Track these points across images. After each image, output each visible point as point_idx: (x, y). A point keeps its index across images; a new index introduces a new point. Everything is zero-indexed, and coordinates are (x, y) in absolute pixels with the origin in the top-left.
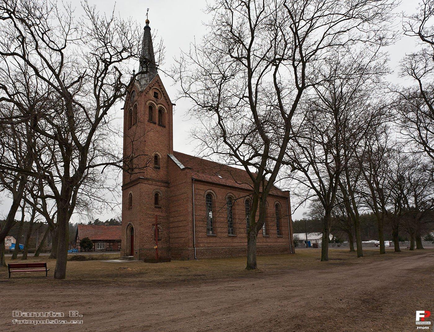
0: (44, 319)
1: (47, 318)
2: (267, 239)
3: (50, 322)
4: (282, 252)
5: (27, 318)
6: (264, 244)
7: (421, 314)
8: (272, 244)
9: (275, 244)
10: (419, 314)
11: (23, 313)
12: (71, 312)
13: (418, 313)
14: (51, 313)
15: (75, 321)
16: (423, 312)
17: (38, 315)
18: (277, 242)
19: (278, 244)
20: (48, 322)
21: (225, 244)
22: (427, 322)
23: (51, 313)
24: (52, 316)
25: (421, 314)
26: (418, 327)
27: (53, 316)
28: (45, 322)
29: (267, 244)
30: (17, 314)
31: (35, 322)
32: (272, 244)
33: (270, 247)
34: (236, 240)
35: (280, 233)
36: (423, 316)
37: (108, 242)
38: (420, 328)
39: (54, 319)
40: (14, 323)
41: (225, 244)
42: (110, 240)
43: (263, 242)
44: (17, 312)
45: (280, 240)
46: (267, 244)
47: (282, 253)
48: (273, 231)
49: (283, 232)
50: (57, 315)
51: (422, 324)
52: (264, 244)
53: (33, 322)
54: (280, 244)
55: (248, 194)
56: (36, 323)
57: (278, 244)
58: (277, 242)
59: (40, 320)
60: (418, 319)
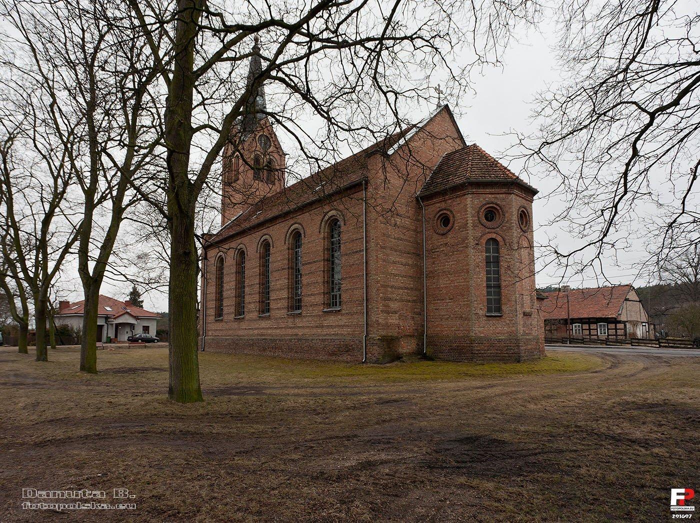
0: (75, 501)
1: (78, 500)
2: (297, 320)
3: (84, 506)
4: (333, 354)
5: (45, 501)
6: (290, 331)
7: (678, 494)
8: (306, 331)
9: (314, 331)
10: (676, 495)
11: (40, 492)
12: (116, 491)
13: (674, 492)
14: (84, 492)
15: (123, 505)
16: (683, 491)
17: (63, 495)
18: (323, 326)
19: (326, 331)
20: (79, 507)
21: (231, 332)
22: (689, 507)
23: (84, 492)
24: (61, 492)
25: (678, 494)
26: (674, 515)
27: (87, 497)
28: (74, 506)
29: (296, 331)
30: (30, 492)
31: (59, 506)
32: (306, 331)
33: (299, 340)
34: (244, 325)
35: (333, 300)
36: (682, 497)
37: (586, 323)
38: (677, 516)
39: (86, 501)
40: (25, 507)
41: (231, 332)
42: (589, 319)
43: (287, 328)
44: (29, 490)
45: (332, 320)
46: (296, 331)
47: (334, 358)
48: (312, 299)
49: (345, 297)
50: (95, 495)
51: (680, 510)
52: (290, 331)
53: (55, 506)
54: (332, 331)
55: (102, 172)
56: (61, 508)
57: (326, 331)
58: (323, 326)
59: (56, 503)
60: (673, 502)
